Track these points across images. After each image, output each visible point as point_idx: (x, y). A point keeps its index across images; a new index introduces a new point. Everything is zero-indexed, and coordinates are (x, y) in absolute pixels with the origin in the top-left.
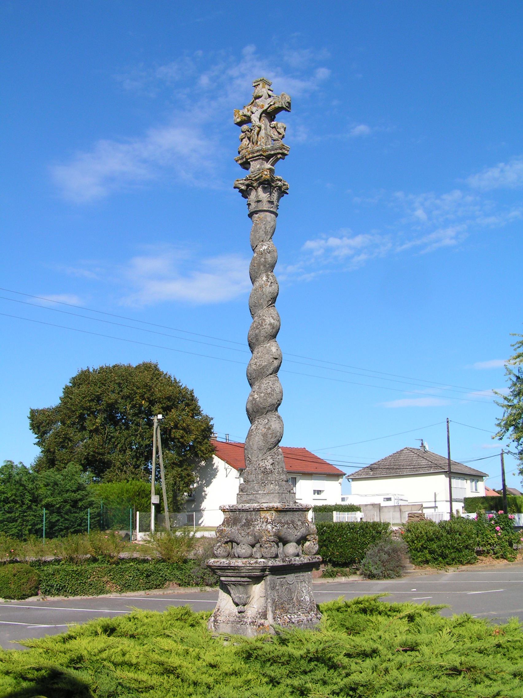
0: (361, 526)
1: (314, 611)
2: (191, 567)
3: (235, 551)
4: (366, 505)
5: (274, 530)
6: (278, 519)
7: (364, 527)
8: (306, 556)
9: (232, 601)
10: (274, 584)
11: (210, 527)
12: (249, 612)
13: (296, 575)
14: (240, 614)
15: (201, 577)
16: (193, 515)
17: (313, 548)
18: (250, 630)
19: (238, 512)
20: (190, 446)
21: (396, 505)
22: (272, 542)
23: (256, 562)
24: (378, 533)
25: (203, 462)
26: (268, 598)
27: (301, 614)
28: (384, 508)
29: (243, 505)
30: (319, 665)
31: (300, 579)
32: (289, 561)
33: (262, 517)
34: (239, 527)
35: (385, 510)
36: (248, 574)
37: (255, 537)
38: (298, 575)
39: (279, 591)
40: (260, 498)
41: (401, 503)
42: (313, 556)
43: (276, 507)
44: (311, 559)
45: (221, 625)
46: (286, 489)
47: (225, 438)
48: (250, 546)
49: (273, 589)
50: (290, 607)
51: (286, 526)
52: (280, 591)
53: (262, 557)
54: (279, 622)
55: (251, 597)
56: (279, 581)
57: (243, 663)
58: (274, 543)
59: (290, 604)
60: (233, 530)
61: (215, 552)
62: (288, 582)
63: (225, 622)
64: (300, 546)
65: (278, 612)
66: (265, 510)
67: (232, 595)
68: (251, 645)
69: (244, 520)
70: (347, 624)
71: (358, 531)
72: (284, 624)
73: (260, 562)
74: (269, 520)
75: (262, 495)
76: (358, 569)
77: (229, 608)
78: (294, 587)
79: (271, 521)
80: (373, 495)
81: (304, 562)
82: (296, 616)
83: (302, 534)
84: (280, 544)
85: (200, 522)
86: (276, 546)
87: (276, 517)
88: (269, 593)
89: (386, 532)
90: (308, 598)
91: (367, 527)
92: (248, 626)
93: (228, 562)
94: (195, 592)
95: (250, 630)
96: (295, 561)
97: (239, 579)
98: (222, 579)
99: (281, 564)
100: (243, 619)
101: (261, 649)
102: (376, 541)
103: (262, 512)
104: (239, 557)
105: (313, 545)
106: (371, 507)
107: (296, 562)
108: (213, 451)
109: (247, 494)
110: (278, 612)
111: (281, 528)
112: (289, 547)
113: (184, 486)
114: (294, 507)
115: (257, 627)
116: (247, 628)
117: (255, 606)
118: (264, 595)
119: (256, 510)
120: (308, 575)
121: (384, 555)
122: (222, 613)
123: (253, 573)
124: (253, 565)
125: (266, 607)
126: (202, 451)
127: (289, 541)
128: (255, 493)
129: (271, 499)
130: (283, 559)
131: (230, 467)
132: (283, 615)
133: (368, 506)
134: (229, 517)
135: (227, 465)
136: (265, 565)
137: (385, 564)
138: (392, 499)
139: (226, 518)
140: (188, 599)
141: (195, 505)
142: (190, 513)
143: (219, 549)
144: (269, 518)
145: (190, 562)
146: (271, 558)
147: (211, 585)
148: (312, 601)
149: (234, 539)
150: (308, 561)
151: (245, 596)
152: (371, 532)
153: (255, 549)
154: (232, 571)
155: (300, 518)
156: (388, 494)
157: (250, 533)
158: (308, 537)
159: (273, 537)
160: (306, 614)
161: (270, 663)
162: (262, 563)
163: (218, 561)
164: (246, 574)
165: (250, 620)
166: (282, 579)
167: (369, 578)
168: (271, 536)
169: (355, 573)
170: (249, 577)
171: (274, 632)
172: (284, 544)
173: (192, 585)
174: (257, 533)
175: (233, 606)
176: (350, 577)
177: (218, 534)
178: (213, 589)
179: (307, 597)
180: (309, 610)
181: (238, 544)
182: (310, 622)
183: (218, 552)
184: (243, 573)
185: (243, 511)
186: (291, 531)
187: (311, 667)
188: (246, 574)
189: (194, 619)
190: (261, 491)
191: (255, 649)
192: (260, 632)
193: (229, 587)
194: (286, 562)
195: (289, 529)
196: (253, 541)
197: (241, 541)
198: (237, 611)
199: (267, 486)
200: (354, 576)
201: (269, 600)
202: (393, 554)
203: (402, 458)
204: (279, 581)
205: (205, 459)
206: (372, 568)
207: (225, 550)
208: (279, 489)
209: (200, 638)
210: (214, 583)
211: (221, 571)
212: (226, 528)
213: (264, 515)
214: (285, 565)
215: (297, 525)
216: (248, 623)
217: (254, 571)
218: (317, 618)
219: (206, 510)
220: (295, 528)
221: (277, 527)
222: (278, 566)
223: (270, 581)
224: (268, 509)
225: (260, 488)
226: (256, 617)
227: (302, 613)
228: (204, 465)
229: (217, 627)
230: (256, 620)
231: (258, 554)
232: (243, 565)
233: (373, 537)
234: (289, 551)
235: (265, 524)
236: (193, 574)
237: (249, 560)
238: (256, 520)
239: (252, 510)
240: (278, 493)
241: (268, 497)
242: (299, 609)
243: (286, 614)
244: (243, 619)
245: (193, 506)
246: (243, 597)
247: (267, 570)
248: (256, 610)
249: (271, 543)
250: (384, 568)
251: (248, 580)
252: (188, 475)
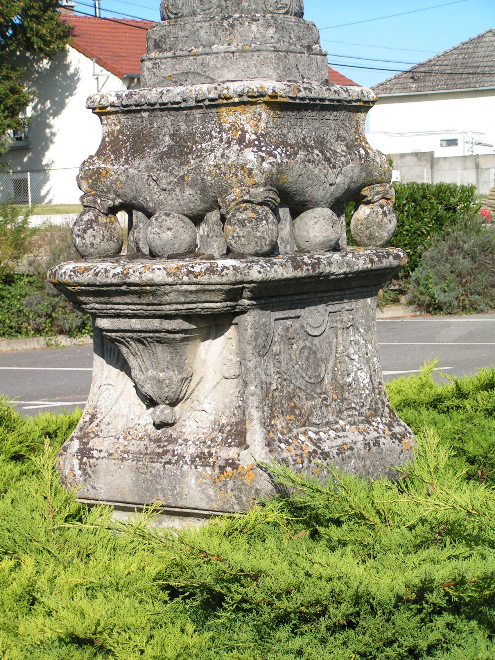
0: (411, 195)
1: (382, 416)
2: (23, 293)
3: (141, 236)
4: (403, 156)
5: (265, 165)
6: (275, 132)
7: (418, 196)
8: (361, 251)
9: (134, 390)
10: (267, 335)
11: (65, 205)
12: (187, 423)
13: (330, 308)
14: (160, 431)
15: (47, 314)
16: (26, 180)
17: (380, 225)
18: (193, 481)
19: (145, 114)
20: (14, 26)
21: (467, 154)
22: (260, 204)
23: (211, 270)
24: (449, 209)
25: (45, 61)
26: (248, 380)
27: (348, 427)
28: (442, 162)
29: (164, 89)
30: (459, 625)
31: (342, 321)
32: (314, 266)
33: (227, 126)
34: (150, 161)
35: (445, 165)
36: (186, 306)
37: (204, 190)
38: (337, 307)
39: (281, 357)
40: (216, 68)
41: (479, 150)
42: (380, 250)
43: (270, 92)
44: (376, 259)
45: (103, 464)
46: (299, 38)
47: (94, 14)
48: (187, 220)
49: (263, 352)
50: (314, 407)
51: (301, 155)
52: (284, 357)
53: (229, 253)
54: (285, 455)
55: (195, 379)
56: (280, 328)
57: (190, 628)
58: (267, 208)
59: (313, 398)
60: (131, 171)
61: (78, 240)
62: (309, 330)
63: (116, 456)
64: (343, 218)
65: (279, 423)
66: (235, 104)
67: (135, 373)
68: (221, 565)
69: (167, 138)
70: (470, 447)
71: (404, 205)
72: (299, 460)
73: (224, 268)
74: (247, 136)
75: (225, 58)
76: (402, 292)
77: (125, 411)
78: (324, 345)
79: (254, 137)
80: (418, 134)
81: (356, 268)
82: (332, 433)
83: (347, 181)
84: (284, 212)
85: (43, 193)
86: (271, 217)
87: (271, 124)
88: (251, 365)
89: (467, 208)
90: (364, 378)
91: (424, 197)
92: (185, 467)
93: (119, 270)
94: (34, 349)
95: (192, 481)
96: (330, 264)
97: (156, 324)
98: (103, 323)
99: (288, 273)
100: (170, 447)
101: (256, 575)
102: (444, 228)
103: (224, 109)
104: (153, 255)
105: (380, 216)
106: (414, 159)
107: (334, 269)
108: (67, 36)
109: (175, 57)
110: (279, 423)
111: (286, 160)
112: (311, 222)
113: (6, 114)
114: (326, 95)
115: (217, 471)
116: (183, 475)
117: (207, 407)
118: (237, 372)
119: (207, 103)
120: (365, 307)
121: (462, 261)
122: (103, 427)
123: (201, 305)
124: (200, 279)
125: (243, 409)
126: (41, 37)
127: (310, 201)
128: (200, 50)
129: (254, 70)
130: (293, 259)
131: (105, 72)
132: (295, 431)
133: (407, 158)
134: (120, 132)
135: (98, 69)
136: (239, 278)
137: (464, 280)
138: (459, 142)
139: (110, 134)
140: (18, 366)
141: (29, 158)
142: (20, 176)
143: (90, 231)
144: (247, 127)
145: (21, 280)
146: (257, 255)
147: (69, 333)
148: (376, 384)
149: (135, 198)
150: (369, 266)
151: (176, 377)
152: (433, 208)
153: (203, 229)
154: (135, 299)
155: (342, 133)
156: (450, 132)
157: (189, 179)
158: (365, 192)
159: (262, 189)
160: (361, 426)
161: (288, 628)
162: (231, 272)
163: (87, 270)
164: (180, 307)
165: (192, 450)
166: (289, 322)
167: (429, 312)
168: (256, 185)
169: (396, 301)
170: (187, 317)
171: (270, 487)
172: (295, 215)
173: (27, 333)
174: (209, 178)
175: (140, 406)
176: (385, 309)
177: (85, 186)
178: (75, 341)
179: (363, 375)
180: (369, 413)
181: (149, 215)
182: (374, 449)
183: (87, 242)
184: (170, 304)
185: (164, 108)
186: (316, 171)
187: (434, 636)
188: (180, 307)
189: (20, 439)
190: (220, 42)
191: (235, 579)
192: (225, 485)
193: (124, 349)
194: (305, 268)
195: (310, 166)
196: (198, 205)
197: (160, 203)
198: (150, 420)
199: (238, 28)
200: (393, 307)
201: (253, 388)
202: (481, 257)
203: (481, 51)
204: (280, 328)
205: (50, 56)
206: (435, 290)
207: (107, 234)
208: (276, 36)
209: (36, 515)
210: (77, 327)
211: (98, 299)
212: (109, 166)
213: (231, 119)
214: (301, 278)
215: (335, 152)
216: (188, 459)
217: (204, 297)
218: (394, 436)
219: (54, 166)
220: (328, 160)
221: (275, 156)
222: (280, 281)
223: (253, 327)
224: (245, 99)
225: (215, 34)
226: (213, 440)
227: (350, 424)
228: (48, 67)
229: (89, 470)
230: (213, 450)
231: (215, 245)
232: (170, 280)
233: (439, 221)
234: (312, 235)
235: (235, 147)
236: (29, 309)
237: (187, 262)
238: (206, 136)
239: (194, 104)
240: (276, 50)
241: (242, 63)
242: (341, 412)
243: (303, 429)
244: (170, 447)
245: (25, 159)
246: (171, 379)
247: (246, 294)
248: (212, 418)
249: (258, 208)
250: (461, 290)
251: (186, 325)
252: (13, 91)
